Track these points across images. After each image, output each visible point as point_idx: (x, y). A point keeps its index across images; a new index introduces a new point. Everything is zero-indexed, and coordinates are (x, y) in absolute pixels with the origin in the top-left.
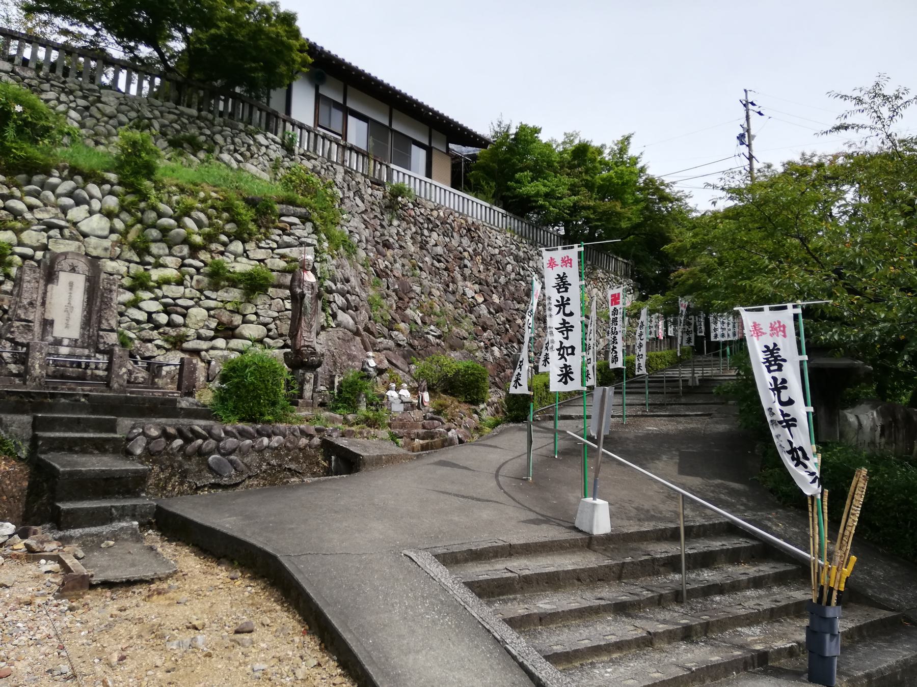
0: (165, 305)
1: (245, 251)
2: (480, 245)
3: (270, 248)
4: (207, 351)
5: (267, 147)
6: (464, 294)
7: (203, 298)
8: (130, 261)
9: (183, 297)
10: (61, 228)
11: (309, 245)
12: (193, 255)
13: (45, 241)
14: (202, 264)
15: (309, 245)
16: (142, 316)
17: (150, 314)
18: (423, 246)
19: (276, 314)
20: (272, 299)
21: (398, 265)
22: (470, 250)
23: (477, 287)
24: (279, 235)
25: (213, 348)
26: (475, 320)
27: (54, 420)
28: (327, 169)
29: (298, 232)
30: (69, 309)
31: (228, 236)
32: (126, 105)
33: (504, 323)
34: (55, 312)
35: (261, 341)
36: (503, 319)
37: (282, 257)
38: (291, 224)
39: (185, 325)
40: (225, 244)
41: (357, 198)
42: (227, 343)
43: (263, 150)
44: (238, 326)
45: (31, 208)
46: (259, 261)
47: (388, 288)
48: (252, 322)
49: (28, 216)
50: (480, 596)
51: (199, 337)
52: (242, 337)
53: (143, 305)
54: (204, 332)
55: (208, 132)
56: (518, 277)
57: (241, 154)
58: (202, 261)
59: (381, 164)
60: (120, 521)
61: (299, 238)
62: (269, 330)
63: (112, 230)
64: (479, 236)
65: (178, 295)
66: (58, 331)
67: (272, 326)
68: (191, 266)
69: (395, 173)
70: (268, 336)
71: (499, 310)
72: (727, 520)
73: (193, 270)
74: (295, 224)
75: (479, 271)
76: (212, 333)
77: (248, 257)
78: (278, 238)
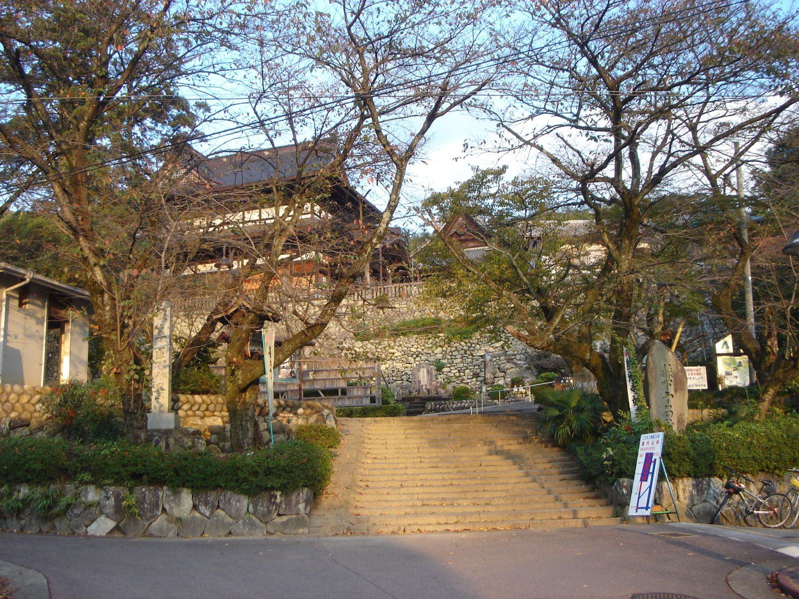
66: (422, 383)
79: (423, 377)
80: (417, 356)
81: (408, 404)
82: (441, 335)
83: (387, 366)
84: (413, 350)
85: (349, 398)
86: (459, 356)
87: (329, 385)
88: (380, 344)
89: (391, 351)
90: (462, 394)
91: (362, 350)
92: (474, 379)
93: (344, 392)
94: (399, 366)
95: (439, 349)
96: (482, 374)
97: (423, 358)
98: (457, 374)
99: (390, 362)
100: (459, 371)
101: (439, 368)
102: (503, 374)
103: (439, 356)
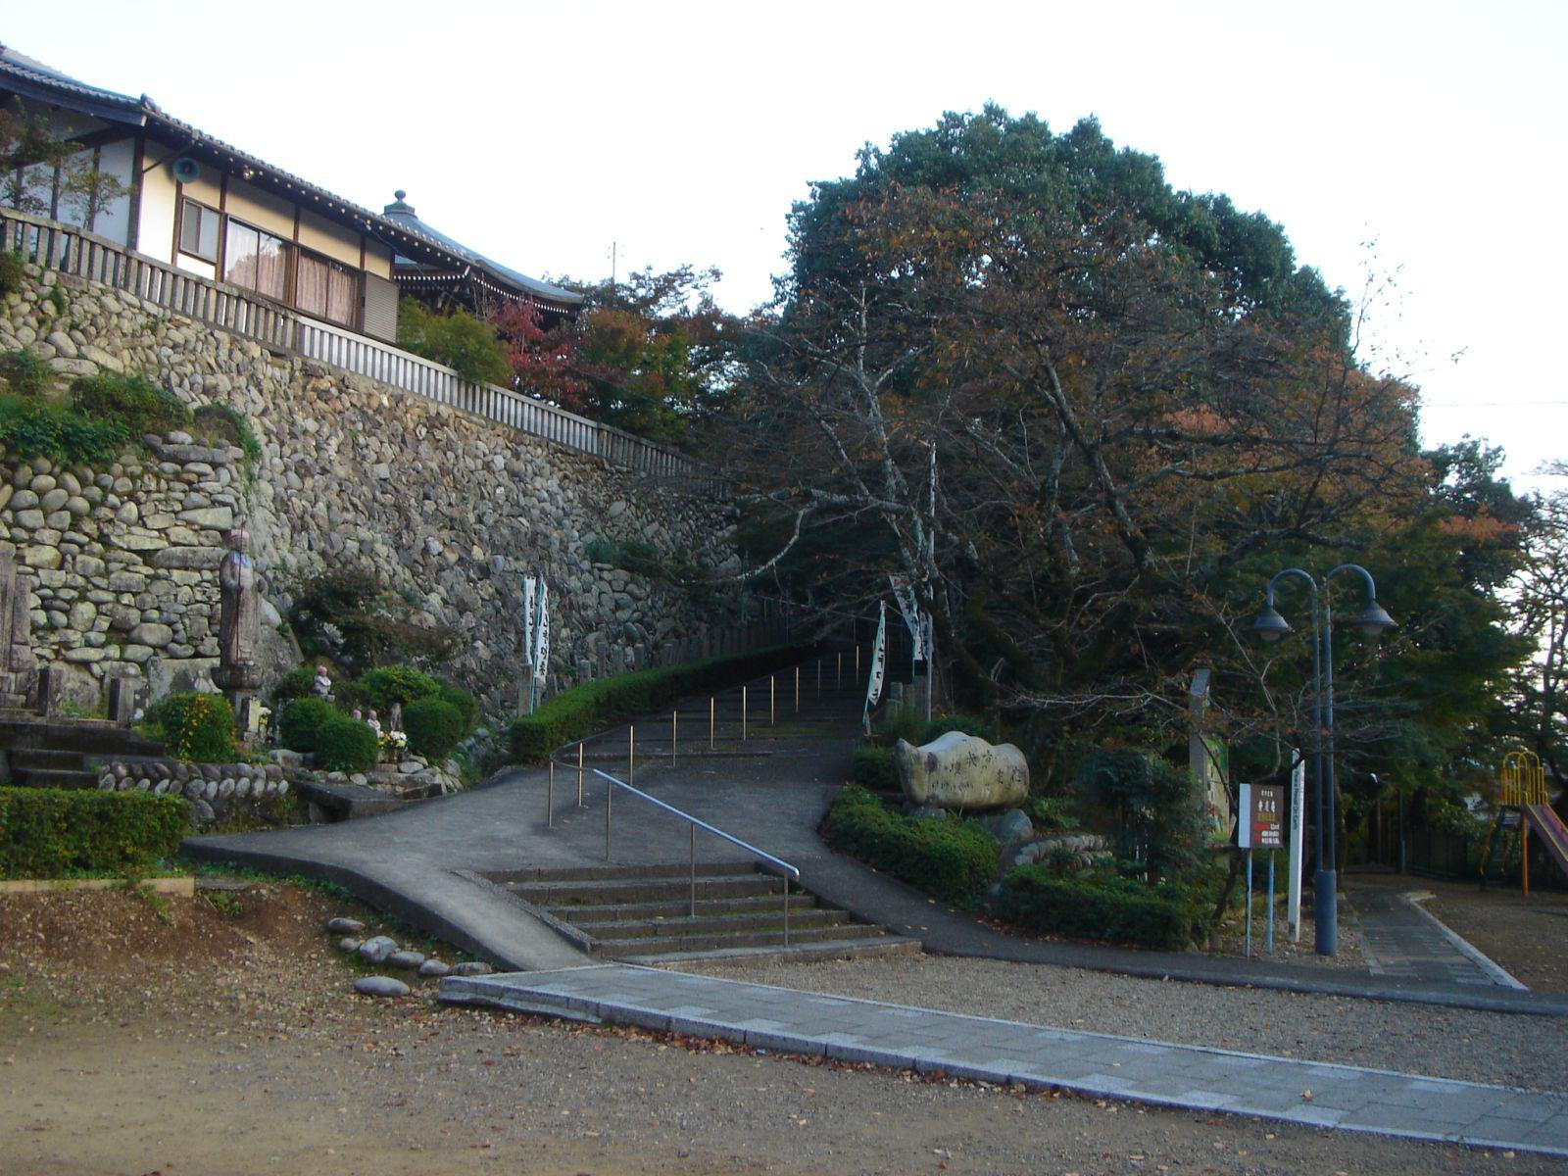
1: (141, 517)
2: (449, 454)
3: (173, 512)
5: (119, 315)
6: (426, 551)
7: (90, 586)
9: (66, 586)
11: (224, 504)
12: (75, 526)
15: (224, 504)
18: (358, 460)
19: (184, 609)
20: (178, 586)
21: (321, 505)
22: (434, 465)
23: (446, 534)
24: (184, 492)
25: (106, 659)
26: (445, 595)
28: (205, 342)
29: (210, 486)
31: (118, 495)
33: (492, 598)
35: (164, 648)
36: (491, 590)
37: (189, 523)
38: (200, 475)
39: (69, 627)
40: (114, 508)
41: (251, 388)
42: (122, 651)
43: (114, 320)
44: (134, 628)
46: (158, 530)
47: (310, 548)
48: (152, 621)
50: (494, 882)
51: (89, 644)
52: (141, 642)
55: (32, 296)
56: (516, 510)
57: (83, 331)
58: (86, 534)
59: (285, 318)
60: (74, 875)
62: (175, 632)
64: (448, 438)
65: (58, 584)
67: (180, 626)
68: (71, 541)
69: (307, 331)
70: (174, 641)
71: (485, 572)
72: (650, 790)
73: (75, 548)
74: (205, 475)
75: (450, 504)
76: (102, 638)
77: (144, 525)
78: (181, 496)
86: (49, 536)
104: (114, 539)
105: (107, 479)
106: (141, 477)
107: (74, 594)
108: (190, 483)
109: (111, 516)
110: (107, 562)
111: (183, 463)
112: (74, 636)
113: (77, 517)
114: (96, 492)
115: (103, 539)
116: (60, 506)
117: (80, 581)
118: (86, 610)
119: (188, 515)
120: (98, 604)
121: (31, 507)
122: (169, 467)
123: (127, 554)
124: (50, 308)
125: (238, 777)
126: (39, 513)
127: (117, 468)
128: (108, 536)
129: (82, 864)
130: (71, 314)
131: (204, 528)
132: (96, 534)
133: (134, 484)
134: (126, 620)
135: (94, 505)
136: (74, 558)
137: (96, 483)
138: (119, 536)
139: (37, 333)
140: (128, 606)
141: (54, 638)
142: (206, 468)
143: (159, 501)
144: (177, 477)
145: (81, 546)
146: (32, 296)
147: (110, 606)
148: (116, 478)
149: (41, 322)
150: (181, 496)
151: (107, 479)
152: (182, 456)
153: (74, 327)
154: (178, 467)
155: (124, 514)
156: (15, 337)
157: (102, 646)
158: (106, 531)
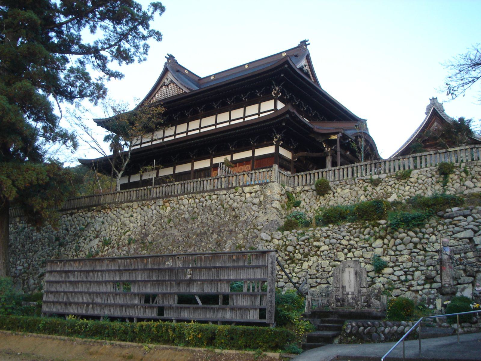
0: (405, 272)
4: (421, 290)
7: (419, 266)
8: (391, 255)
10: (366, 248)
12: (415, 247)
13: (361, 254)
14: (419, 250)
16: (396, 278)
17: (399, 276)
24: (453, 228)
27: (335, 323)
30: (350, 281)
31: (429, 234)
32: (421, 174)
34: (346, 284)
37: (455, 238)
38: (459, 220)
39: (413, 280)
45: (357, 242)
49: (356, 246)
51: (418, 285)
53: (395, 273)
54: (419, 282)
57: (476, 178)
58: (419, 249)
61: (463, 226)
63: (384, 244)
65: (409, 267)
66: (348, 289)
79: (349, 281)
80: (350, 251)
81: (318, 321)
82: (382, 222)
83: (310, 263)
84: (344, 242)
85: (232, 309)
86: (405, 252)
87: (209, 290)
88: (303, 234)
89: (315, 243)
90: (402, 310)
91: (281, 242)
92: (427, 286)
93: (226, 299)
94: (325, 263)
95: (379, 242)
96: (438, 279)
97: (358, 253)
98: (403, 278)
99: (314, 259)
100: (406, 274)
101: (379, 267)
102: (471, 279)
103: (379, 251)
104: (427, 249)
105: (424, 230)
106: (436, 227)
107: (414, 269)
108: (455, 224)
109: (427, 241)
110: (425, 256)
111: (452, 218)
112: (413, 282)
113: (415, 244)
114: (420, 235)
115: (425, 250)
116: (409, 242)
117: (416, 264)
118: (417, 274)
119: (454, 236)
120: (421, 271)
121: (400, 244)
122: (447, 221)
123: (431, 253)
124: (463, 175)
125: (399, 326)
126: (402, 246)
127: (427, 226)
128: (425, 248)
129: (246, 347)
130: (471, 174)
131: (461, 239)
132: (422, 249)
133: (433, 229)
134: (430, 275)
135: (421, 239)
136: (415, 257)
137: (421, 232)
138: (429, 248)
139: (460, 184)
140: (431, 270)
141: (407, 284)
142: (462, 218)
143: (443, 233)
144: (451, 223)
145: (417, 253)
146: (458, 173)
147: (425, 271)
148: (427, 229)
149: (461, 180)
150: (452, 229)
151: (424, 230)
152: (451, 216)
153: (473, 178)
154: (451, 220)
155: (430, 240)
156: (453, 188)
157: (423, 285)
158: (425, 247)
